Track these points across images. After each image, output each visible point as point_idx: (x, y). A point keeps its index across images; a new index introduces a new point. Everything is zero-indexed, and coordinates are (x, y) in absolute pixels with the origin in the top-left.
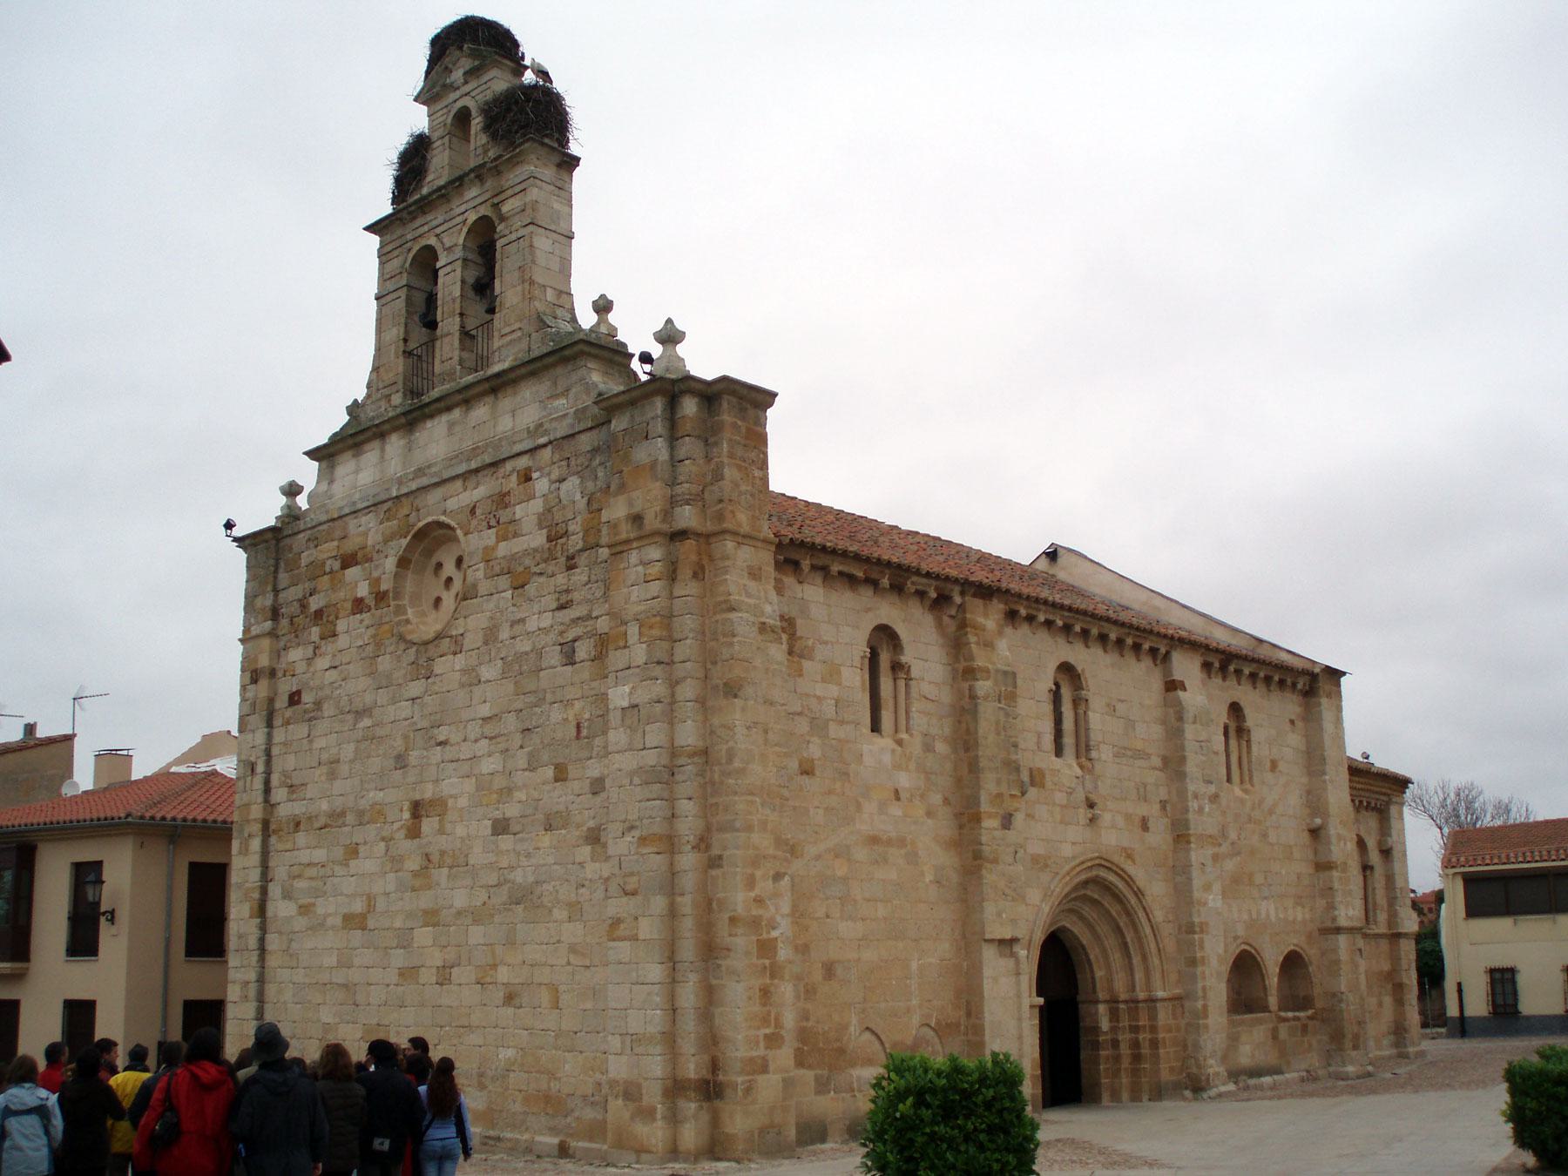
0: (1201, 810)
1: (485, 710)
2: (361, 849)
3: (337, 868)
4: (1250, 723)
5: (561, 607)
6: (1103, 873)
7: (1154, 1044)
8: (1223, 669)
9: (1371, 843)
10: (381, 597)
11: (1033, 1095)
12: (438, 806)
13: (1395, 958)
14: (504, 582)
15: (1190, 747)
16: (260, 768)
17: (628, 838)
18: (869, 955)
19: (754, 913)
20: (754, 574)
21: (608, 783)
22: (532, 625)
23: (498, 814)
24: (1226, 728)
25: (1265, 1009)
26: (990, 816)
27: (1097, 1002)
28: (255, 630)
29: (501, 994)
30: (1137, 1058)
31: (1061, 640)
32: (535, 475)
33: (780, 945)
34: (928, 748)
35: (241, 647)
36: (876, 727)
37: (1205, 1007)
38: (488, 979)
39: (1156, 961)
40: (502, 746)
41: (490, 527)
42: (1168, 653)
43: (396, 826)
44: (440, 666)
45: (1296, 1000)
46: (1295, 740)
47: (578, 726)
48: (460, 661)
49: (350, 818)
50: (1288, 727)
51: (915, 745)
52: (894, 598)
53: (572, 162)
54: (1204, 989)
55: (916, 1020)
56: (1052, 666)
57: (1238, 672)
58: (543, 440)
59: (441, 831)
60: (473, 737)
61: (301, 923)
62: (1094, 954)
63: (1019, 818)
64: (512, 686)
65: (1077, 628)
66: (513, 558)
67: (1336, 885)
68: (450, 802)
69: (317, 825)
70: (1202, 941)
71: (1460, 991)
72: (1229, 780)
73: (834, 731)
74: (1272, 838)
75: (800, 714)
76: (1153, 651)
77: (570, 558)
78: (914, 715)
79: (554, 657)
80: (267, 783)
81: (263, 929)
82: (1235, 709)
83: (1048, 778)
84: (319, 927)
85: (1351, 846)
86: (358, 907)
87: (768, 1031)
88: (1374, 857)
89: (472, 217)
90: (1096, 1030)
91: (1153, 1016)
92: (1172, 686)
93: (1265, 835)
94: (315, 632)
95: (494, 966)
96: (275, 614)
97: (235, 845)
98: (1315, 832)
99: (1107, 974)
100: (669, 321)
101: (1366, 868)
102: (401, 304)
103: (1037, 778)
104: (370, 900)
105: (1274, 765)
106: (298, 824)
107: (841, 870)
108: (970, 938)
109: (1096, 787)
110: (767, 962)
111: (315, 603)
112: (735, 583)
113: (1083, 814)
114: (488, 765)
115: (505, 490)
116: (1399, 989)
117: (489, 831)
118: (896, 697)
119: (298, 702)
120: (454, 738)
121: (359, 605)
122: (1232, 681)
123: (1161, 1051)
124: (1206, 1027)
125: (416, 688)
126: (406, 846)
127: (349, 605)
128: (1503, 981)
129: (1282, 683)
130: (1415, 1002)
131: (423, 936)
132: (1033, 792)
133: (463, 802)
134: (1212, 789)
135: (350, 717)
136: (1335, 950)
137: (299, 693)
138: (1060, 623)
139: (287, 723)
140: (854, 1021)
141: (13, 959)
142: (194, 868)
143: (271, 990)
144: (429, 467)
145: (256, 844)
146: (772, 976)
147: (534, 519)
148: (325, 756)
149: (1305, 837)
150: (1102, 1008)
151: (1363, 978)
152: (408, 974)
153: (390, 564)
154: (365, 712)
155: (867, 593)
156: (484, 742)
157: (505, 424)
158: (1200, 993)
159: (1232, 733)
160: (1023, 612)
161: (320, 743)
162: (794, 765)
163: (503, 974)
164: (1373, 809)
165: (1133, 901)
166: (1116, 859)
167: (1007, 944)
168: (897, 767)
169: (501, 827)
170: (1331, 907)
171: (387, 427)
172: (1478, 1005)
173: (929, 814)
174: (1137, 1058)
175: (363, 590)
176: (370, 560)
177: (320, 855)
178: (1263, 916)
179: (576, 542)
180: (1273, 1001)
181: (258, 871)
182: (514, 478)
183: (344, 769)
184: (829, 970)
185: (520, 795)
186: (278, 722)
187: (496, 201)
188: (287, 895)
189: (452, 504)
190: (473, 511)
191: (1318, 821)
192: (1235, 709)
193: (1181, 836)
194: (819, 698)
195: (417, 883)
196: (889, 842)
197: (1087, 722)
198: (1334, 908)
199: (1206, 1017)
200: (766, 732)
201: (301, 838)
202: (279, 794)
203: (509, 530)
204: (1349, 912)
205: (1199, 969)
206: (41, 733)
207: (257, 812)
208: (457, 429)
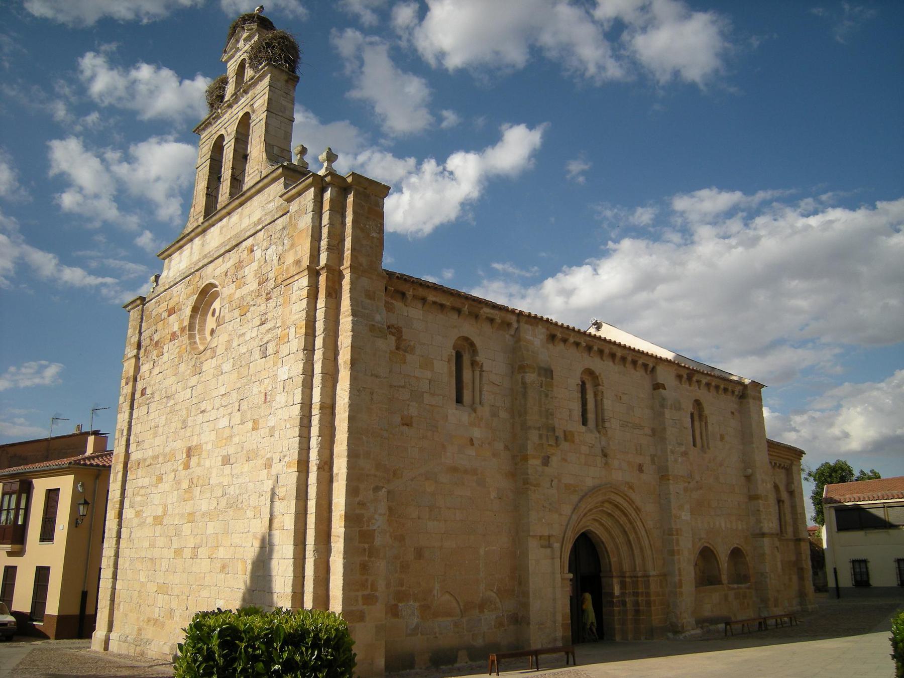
0: (676, 460)
1: (223, 391)
2: (164, 476)
3: (153, 489)
4: (707, 412)
5: (262, 324)
6: (613, 497)
7: (648, 604)
8: (689, 378)
9: (782, 488)
12: (199, 447)
14: (237, 313)
16: (125, 433)
17: (283, 463)
19: (358, 511)
22: (247, 337)
23: (225, 453)
24: (692, 415)
25: (718, 582)
26: (534, 457)
27: (612, 577)
30: (637, 612)
31: (585, 355)
32: (255, 248)
33: (376, 534)
34: (494, 415)
37: (680, 580)
38: (214, 556)
40: (229, 411)
41: (233, 282)
43: (180, 462)
44: (205, 367)
45: (740, 577)
49: (161, 460)
53: (296, 79)
54: (679, 569)
56: (579, 369)
57: (698, 382)
58: (259, 227)
59: (199, 465)
60: (216, 407)
61: (136, 521)
62: (610, 546)
63: (554, 460)
64: (236, 375)
65: (595, 348)
66: (242, 298)
67: (761, 509)
68: (204, 446)
69: (147, 464)
70: (678, 540)
72: (694, 445)
75: (403, 387)
79: (257, 354)
80: (128, 441)
82: (698, 403)
84: (142, 524)
85: (770, 486)
86: (160, 513)
87: (365, 593)
88: (785, 495)
89: (241, 114)
90: (612, 594)
92: (657, 386)
94: (155, 352)
97: (112, 475)
98: (748, 478)
99: (617, 557)
101: (780, 501)
103: (568, 436)
104: (165, 507)
105: (722, 438)
108: (519, 534)
110: (366, 546)
111: (156, 338)
113: (599, 460)
116: (801, 570)
117: (220, 463)
118: (473, 383)
120: (209, 408)
122: (695, 387)
125: (193, 381)
126: (182, 473)
128: (860, 568)
130: (811, 579)
131: (187, 529)
133: (209, 447)
134: (683, 449)
135: (165, 400)
138: (584, 344)
140: (437, 586)
145: (120, 475)
147: (252, 274)
148: (153, 424)
150: (615, 580)
151: (779, 564)
153: (188, 311)
157: (246, 222)
158: (677, 572)
159: (696, 417)
161: (152, 416)
162: (397, 419)
163: (222, 553)
165: (633, 514)
167: (546, 542)
169: (226, 461)
170: (759, 521)
172: (846, 580)
173: (494, 455)
174: (637, 612)
175: (176, 328)
177: (146, 481)
180: (724, 578)
181: (119, 491)
183: (160, 429)
185: (236, 440)
188: (131, 507)
189: (218, 272)
191: (750, 471)
192: (698, 403)
193: (664, 476)
194: (417, 378)
195: (186, 496)
197: (602, 404)
198: (760, 522)
199: (681, 587)
200: (372, 393)
201: (140, 472)
202: (133, 448)
204: (770, 524)
205: (676, 557)
207: (122, 459)
208: (225, 229)
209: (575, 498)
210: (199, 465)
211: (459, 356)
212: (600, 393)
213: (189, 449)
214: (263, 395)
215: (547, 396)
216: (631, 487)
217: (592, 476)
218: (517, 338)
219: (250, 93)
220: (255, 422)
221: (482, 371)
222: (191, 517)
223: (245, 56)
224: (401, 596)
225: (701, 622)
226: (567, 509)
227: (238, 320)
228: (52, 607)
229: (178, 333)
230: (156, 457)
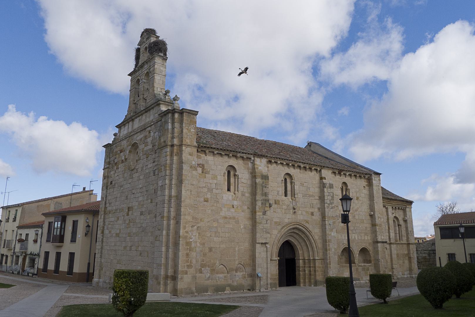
1: (141, 186)
4: (349, 187)
5: (154, 162)
7: (315, 271)
9: (400, 219)
10: (126, 159)
13: (409, 250)
15: (326, 194)
18: (223, 246)
20: (191, 154)
22: (149, 166)
26: (259, 212)
27: (299, 259)
34: (243, 195)
36: (229, 190)
39: (316, 249)
42: (320, 170)
46: (366, 192)
49: (118, 211)
51: (239, 194)
52: (234, 159)
54: (330, 257)
55: (237, 263)
57: (345, 174)
62: (298, 247)
63: (268, 213)
65: (291, 165)
66: (147, 151)
70: (329, 244)
71: (440, 259)
74: (357, 217)
76: (316, 170)
78: (239, 187)
79: (152, 174)
81: (103, 236)
83: (281, 202)
86: (118, 232)
90: (299, 267)
91: (315, 264)
93: (354, 216)
96: (109, 163)
98: (371, 216)
99: (302, 254)
100: (176, 96)
102: (133, 92)
105: (358, 198)
107: (215, 224)
109: (296, 204)
112: (185, 156)
113: (292, 211)
114: (141, 199)
122: (343, 177)
124: (330, 267)
125: (130, 181)
129: (360, 177)
132: (274, 206)
133: (136, 207)
136: (378, 247)
138: (285, 163)
140: (218, 262)
145: (103, 216)
146: (190, 251)
149: (369, 217)
150: (301, 261)
152: (125, 247)
154: (121, 186)
155: (226, 158)
160: (273, 161)
161: (115, 193)
163: (140, 249)
164: (401, 209)
166: (302, 223)
168: (234, 200)
170: (376, 236)
171: (133, 118)
177: (112, 219)
178: (353, 238)
183: (118, 199)
184: (210, 250)
188: (107, 229)
189: (138, 138)
196: (230, 218)
202: (108, 205)
206: (86, 190)
209: (279, 227)
210: (132, 214)
211: (229, 172)
213: (129, 208)
215: (266, 187)
216: (307, 222)
217: (288, 218)
218: (253, 163)
219: (149, 64)
220: (151, 200)
221: (238, 178)
222: (129, 235)
223: (147, 45)
224: (203, 266)
226: (275, 232)
228: (76, 269)
230: (116, 210)
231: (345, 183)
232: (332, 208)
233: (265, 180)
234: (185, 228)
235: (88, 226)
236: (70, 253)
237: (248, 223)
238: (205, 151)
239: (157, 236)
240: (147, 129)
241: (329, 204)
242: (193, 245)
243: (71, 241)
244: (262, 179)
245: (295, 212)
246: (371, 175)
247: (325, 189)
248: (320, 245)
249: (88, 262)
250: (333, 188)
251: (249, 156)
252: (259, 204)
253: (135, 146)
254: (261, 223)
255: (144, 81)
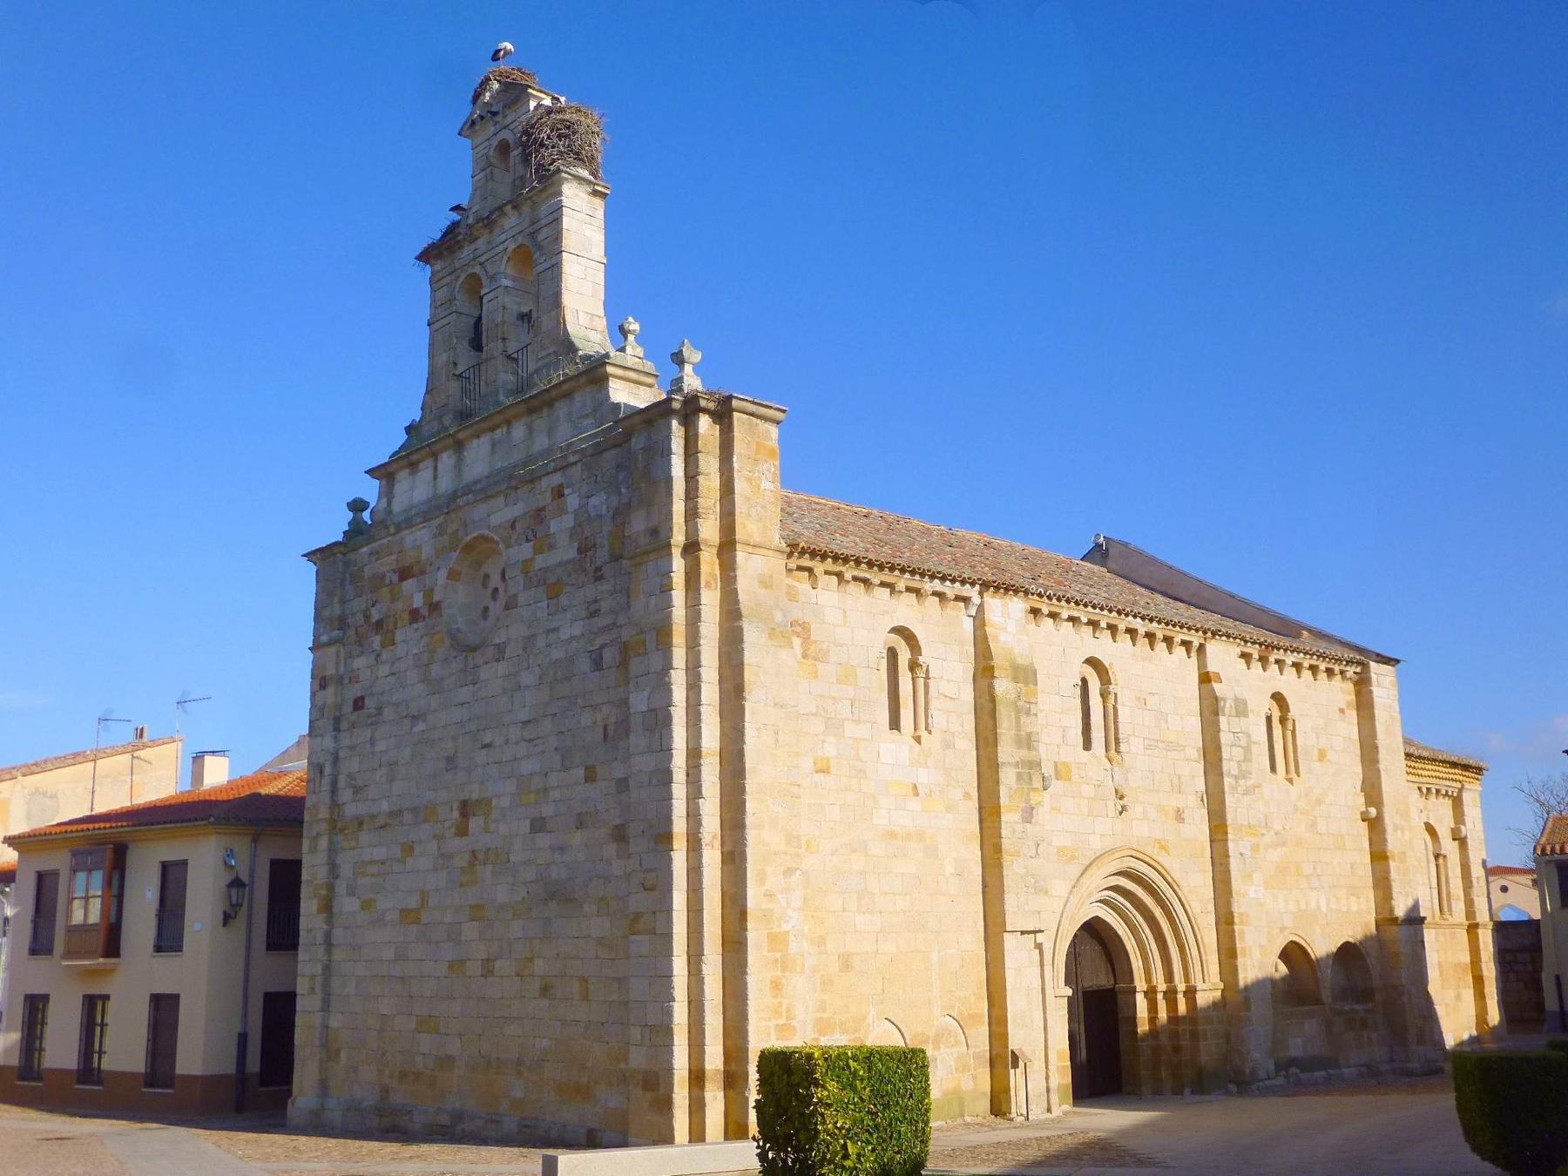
1: (523, 715)
5: (593, 614)
11: (1059, 1085)
12: (484, 804)
21: (632, 783)
22: (565, 634)
24: (1269, 719)
26: (1010, 810)
28: (324, 639)
29: (537, 986)
32: (567, 491)
34: (948, 745)
35: (310, 656)
36: (895, 724)
41: (528, 540)
42: (1202, 646)
43: (446, 825)
44: (485, 673)
46: (1349, 727)
47: (605, 727)
48: (502, 668)
49: (407, 817)
50: (1337, 715)
59: (486, 830)
63: (1041, 814)
65: (1103, 624)
68: (494, 802)
70: (1242, 932)
72: (1273, 768)
73: (851, 730)
74: (1322, 827)
77: (598, 569)
79: (584, 665)
80: (334, 783)
86: (413, 902)
87: (780, 1022)
93: (1314, 825)
95: (531, 960)
103: (1061, 772)
104: (424, 896)
105: (1322, 755)
106: (361, 824)
109: (1127, 779)
110: (778, 955)
111: (375, 615)
113: (1112, 805)
114: (527, 767)
115: (541, 505)
119: (362, 707)
120: (497, 742)
121: (415, 615)
123: (1202, 1043)
125: (464, 694)
127: (406, 616)
131: (470, 931)
132: (1056, 786)
133: (505, 802)
137: (362, 698)
138: (1085, 620)
139: (353, 726)
141: (107, 955)
142: (274, 863)
143: (336, 983)
144: (475, 483)
145: (324, 843)
152: (457, 965)
156: (524, 744)
161: (381, 746)
162: (807, 764)
163: (539, 966)
166: (1148, 851)
169: (538, 825)
175: (418, 601)
176: (423, 573)
177: (379, 853)
178: (1313, 905)
179: (602, 555)
182: (548, 495)
184: (846, 964)
185: (555, 795)
186: (344, 725)
187: (531, 229)
188: (351, 892)
189: (495, 520)
190: (513, 526)
199: (1248, 1009)
201: (365, 837)
202: (345, 795)
203: (544, 544)
209: (1075, 870)
210: (486, 830)
212: (1112, 697)
214: (601, 731)
215: (1028, 713)
218: (979, 621)
221: (927, 678)
222: (476, 912)
225: (1283, 1066)
226: (1060, 888)
227: (544, 604)
229: (425, 611)
230: (396, 814)
231: (1278, 698)
232: (1247, 793)
233: (1027, 683)
234: (762, 879)
235: (236, 883)
236: (27, 997)
237: (973, 854)
238: (810, 570)
239: (637, 917)
240: (545, 482)
241: (1236, 777)
242: (793, 947)
243: (158, 948)
244: (1016, 680)
245: (1124, 808)
246: (1365, 666)
247: (1223, 720)
248: (1210, 938)
249: (237, 1029)
250: (1246, 715)
251: (967, 590)
252: (1008, 777)
253: (477, 550)
254: (1017, 854)
255: (505, 282)
